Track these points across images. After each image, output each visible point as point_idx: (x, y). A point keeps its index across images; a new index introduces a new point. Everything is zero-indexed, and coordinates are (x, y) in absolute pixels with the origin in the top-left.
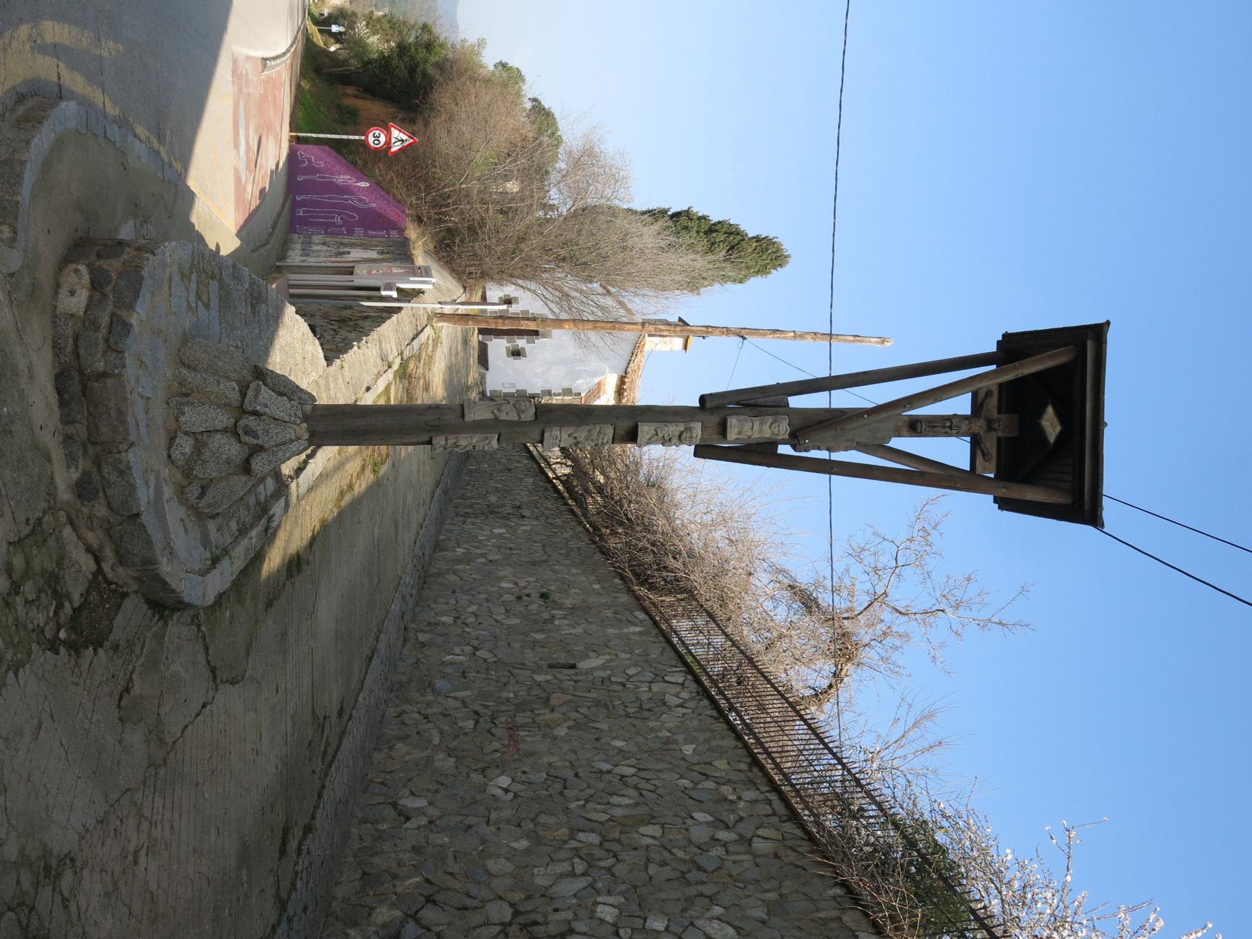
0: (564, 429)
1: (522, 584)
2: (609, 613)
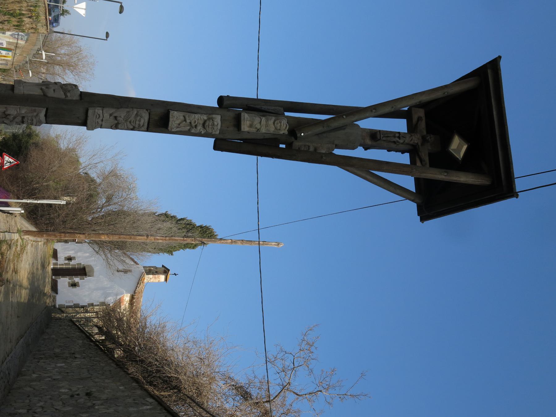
0: (105, 110)
1: (74, 389)
2: (130, 400)
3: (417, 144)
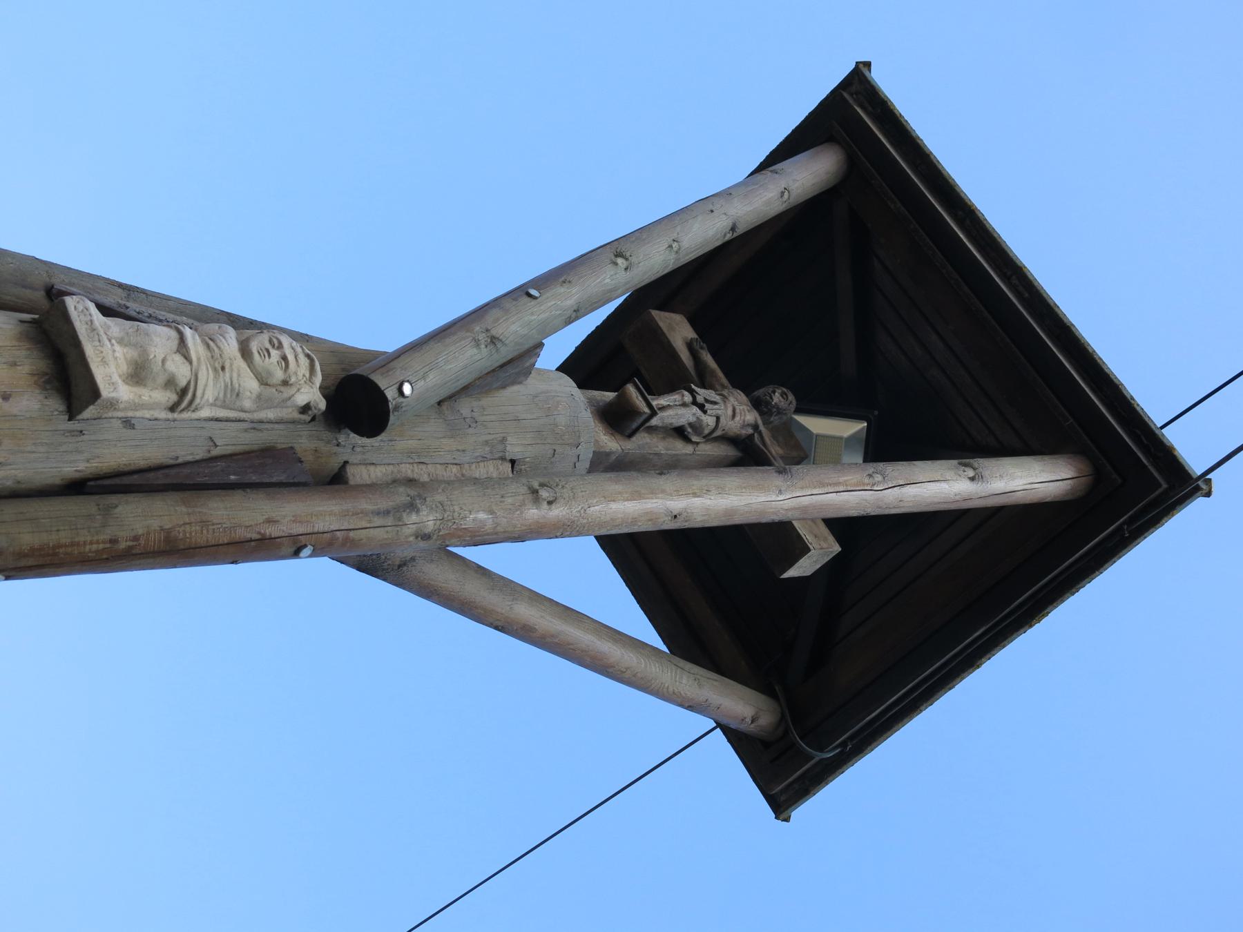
3: (755, 427)
